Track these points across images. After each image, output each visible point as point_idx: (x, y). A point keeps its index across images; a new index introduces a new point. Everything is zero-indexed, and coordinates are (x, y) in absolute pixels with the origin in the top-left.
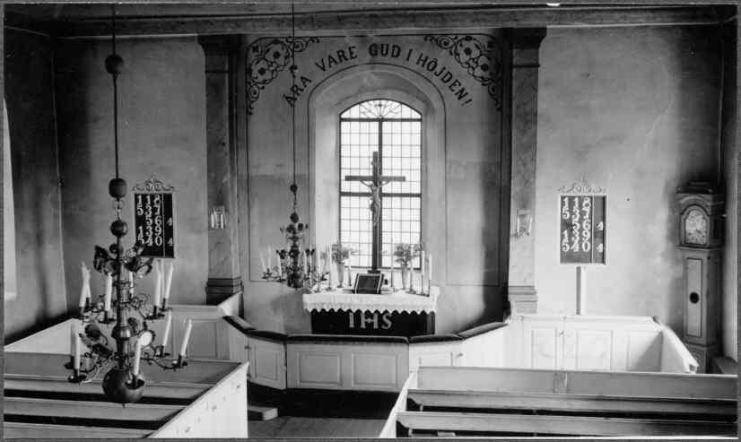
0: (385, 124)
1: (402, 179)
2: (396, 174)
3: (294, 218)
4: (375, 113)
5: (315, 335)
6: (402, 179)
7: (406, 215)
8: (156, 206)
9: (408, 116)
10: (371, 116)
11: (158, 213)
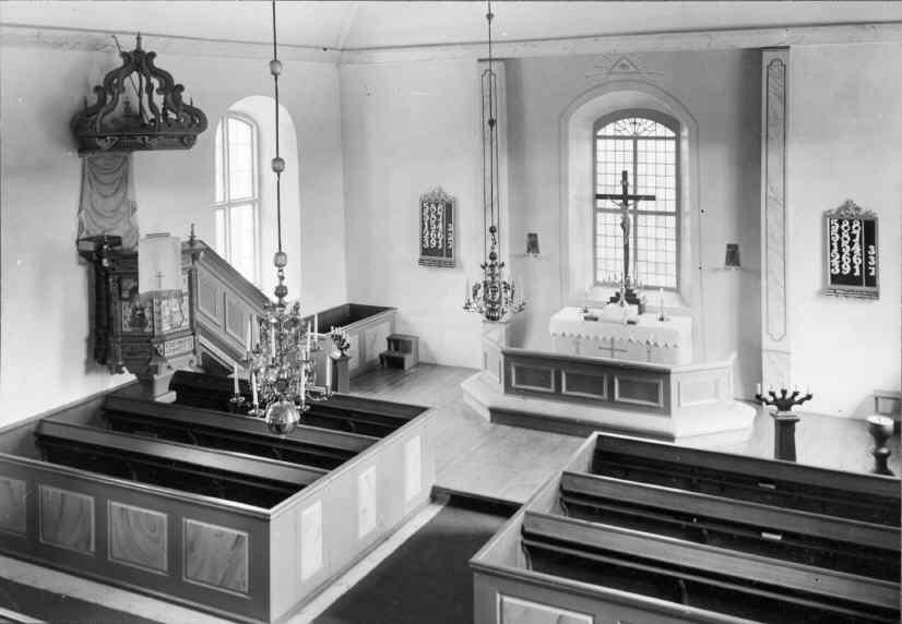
0: (640, 142)
1: (652, 198)
2: (650, 192)
3: (493, 257)
4: (629, 131)
5: (783, 461)
6: (652, 198)
7: (661, 233)
8: (854, 232)
9: (660, 134)
10: (625, 133)
11: (857, 240)
